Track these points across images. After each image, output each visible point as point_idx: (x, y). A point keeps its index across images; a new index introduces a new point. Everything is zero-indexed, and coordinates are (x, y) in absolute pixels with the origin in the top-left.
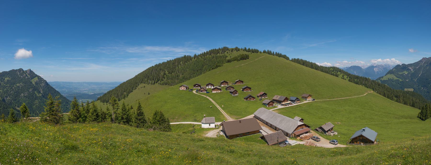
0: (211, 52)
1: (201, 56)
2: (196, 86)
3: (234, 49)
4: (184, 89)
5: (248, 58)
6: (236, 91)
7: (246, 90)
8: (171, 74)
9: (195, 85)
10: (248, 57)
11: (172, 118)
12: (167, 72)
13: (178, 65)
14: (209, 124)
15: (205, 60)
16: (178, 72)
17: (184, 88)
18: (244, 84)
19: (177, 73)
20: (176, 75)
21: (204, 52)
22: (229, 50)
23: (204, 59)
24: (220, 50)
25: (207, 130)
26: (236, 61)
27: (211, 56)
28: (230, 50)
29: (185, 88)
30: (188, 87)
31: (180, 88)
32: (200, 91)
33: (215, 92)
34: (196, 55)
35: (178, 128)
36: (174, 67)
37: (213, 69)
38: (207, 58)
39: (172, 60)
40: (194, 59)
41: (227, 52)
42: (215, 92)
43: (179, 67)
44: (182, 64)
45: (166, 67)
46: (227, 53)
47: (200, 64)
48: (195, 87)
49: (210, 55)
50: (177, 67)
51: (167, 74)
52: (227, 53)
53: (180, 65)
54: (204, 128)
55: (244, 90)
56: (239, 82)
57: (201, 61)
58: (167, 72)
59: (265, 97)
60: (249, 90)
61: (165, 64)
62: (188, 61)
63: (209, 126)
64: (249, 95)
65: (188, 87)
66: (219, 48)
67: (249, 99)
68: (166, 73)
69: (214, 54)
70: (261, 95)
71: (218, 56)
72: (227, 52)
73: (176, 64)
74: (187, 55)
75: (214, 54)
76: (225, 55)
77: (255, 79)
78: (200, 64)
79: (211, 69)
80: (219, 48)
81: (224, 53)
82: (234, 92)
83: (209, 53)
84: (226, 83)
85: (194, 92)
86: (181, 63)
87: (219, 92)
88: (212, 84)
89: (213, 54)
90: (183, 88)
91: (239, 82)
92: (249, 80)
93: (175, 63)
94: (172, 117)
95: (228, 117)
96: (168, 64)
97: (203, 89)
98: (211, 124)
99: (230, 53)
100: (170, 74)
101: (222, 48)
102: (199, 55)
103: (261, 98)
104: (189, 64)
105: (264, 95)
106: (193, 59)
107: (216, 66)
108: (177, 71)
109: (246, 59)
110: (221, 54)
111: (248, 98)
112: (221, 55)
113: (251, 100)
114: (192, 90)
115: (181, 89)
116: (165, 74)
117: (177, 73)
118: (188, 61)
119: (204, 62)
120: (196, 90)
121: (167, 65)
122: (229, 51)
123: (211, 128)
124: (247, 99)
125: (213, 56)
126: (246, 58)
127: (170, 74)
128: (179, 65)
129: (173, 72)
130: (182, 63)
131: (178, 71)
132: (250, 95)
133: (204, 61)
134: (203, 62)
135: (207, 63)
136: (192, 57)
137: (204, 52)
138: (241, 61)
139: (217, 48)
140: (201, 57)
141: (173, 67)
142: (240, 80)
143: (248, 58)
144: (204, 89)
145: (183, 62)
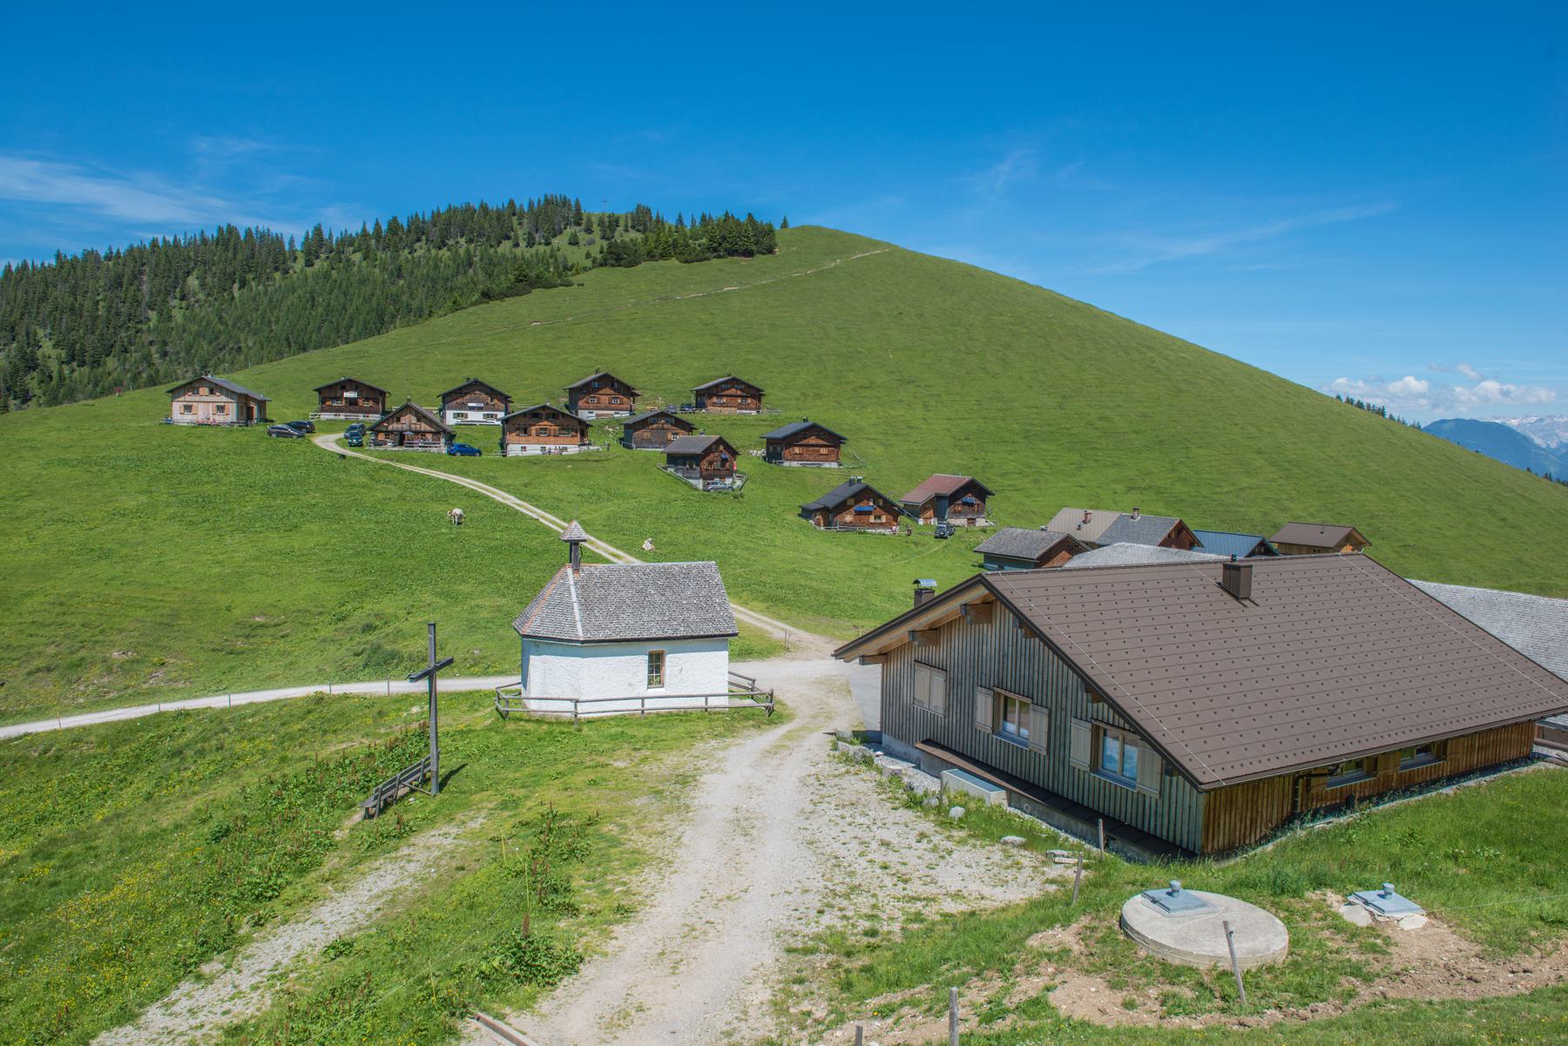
0: (449, 224)
1: (368, 246)
2: (342, 404)
3: (622, 223)
4: (220, 418)
5: (770, 251)
6: (728, 448)
7: (800, 457)
8: (96, 363)
9: (330, 387)
10: (766, 241)
11: (49, 670)
12: (48, 349)
13: (165, 302)
14: (640, 663)
15: (400, 276)
16: (165, 354)
17: (221, 409)
18: (765, 412)
19: (147, 359)
20: (144, 375)
21: (395, 219)
22: (589, 223)
23: (391, 267)
24: (514, 218)
25: (643, 732)
26: (674, 262)
27: (444, 253)
28: (596, 228)
29: (232, 408)
30: (262, 404)
31: (177, 407)
32: (388, 433)
33: (534, 450)
34: (326, 236)
35: (137, 762)
36: (124, 309)
37: (487, 296)
38: (417, 263)
39: (108, 258)
40: (309, 264)
41: (574, 236)
42: (534, 450)
43: (170, 318)
44: (201, 296)
45: (47, 308)
46: (574, 242)
47: (357, 302)
48: (339, 410)
49: (440, 248)
50: (153, 315)
51: (54, 366)
52: (574, 242)
53: (183, 298)
54: (576, 723)
55: (786, 453)
56: (733, 391)
57: (363, 282)
58: (48, 349)
59: (972, 521)
60: (826, 458)
61: (38, 278)
62: (250, 276)
63: (643, 690)
64: (851, 482)
65: (261, 397)
66: (512, 203)
67: (849, 518)
68: (39, 353)
69: (470, 241)
70: (939, 498)
71: (503, 255)
72: (574, 236)
73: (145, 288)
74: (249, 232)
75: (470, 241)
76: (559, 254)
77: (854, 390)
78: (357, 302)
79: (476, 297)
80: (512, 203)
81: (548, 244)
82: (708, 451)
83: (435, 233)
84: (618, 391)
85: (328, 442)
86: (193, 282)
87: (573, 449)
88: (493, 393)
89: (462, 241)
90: (203, 408)
91: (733, 391)
92: (805, 396)
93: (136, 276)
94: (52, 650)
95: (770, 624)
96: (66, 281)
97: (421, 417)
98: (670, 660)
99: (591, 243)
100: (82, 364)
101: (531, 205)
102: (346, 241)
103: (934, 521)
104: (266, 300)
105: (970, 498)
106: (301, 262)
107: (518, 280)
108: (153, 349)
109: (749, 253)
110: (523, 244)
111: (842, 507)
112: (527, 255)
113: (873, 525)
114: (304, 428)
115: (188, 417)
116: (32, 365)
117: (151, 364)
118: (250, 276)
119: (394, 290)
120: (342, 435)
121: (60, 293)
122: (589, 230)
123: (683, 715)
124: (838, 519)
125: (462, 251)
126: (754, 248)
127: (86, 369)
128: (175, 303)
129: (117, 347)
130: (203, 285)
131: (165, 343)
132: (856, 488)
133: (393, 284)
134: (378, 292)
135: (415, 304)
136: (293, 252)
137: (395, 219)
138: (715, 261)
139: (496, 202)
140: (365, 258)
141: (118, 314)
142: (744, 378)
143: (770, 251)
144: (430, 422)
145: (209, 280)
